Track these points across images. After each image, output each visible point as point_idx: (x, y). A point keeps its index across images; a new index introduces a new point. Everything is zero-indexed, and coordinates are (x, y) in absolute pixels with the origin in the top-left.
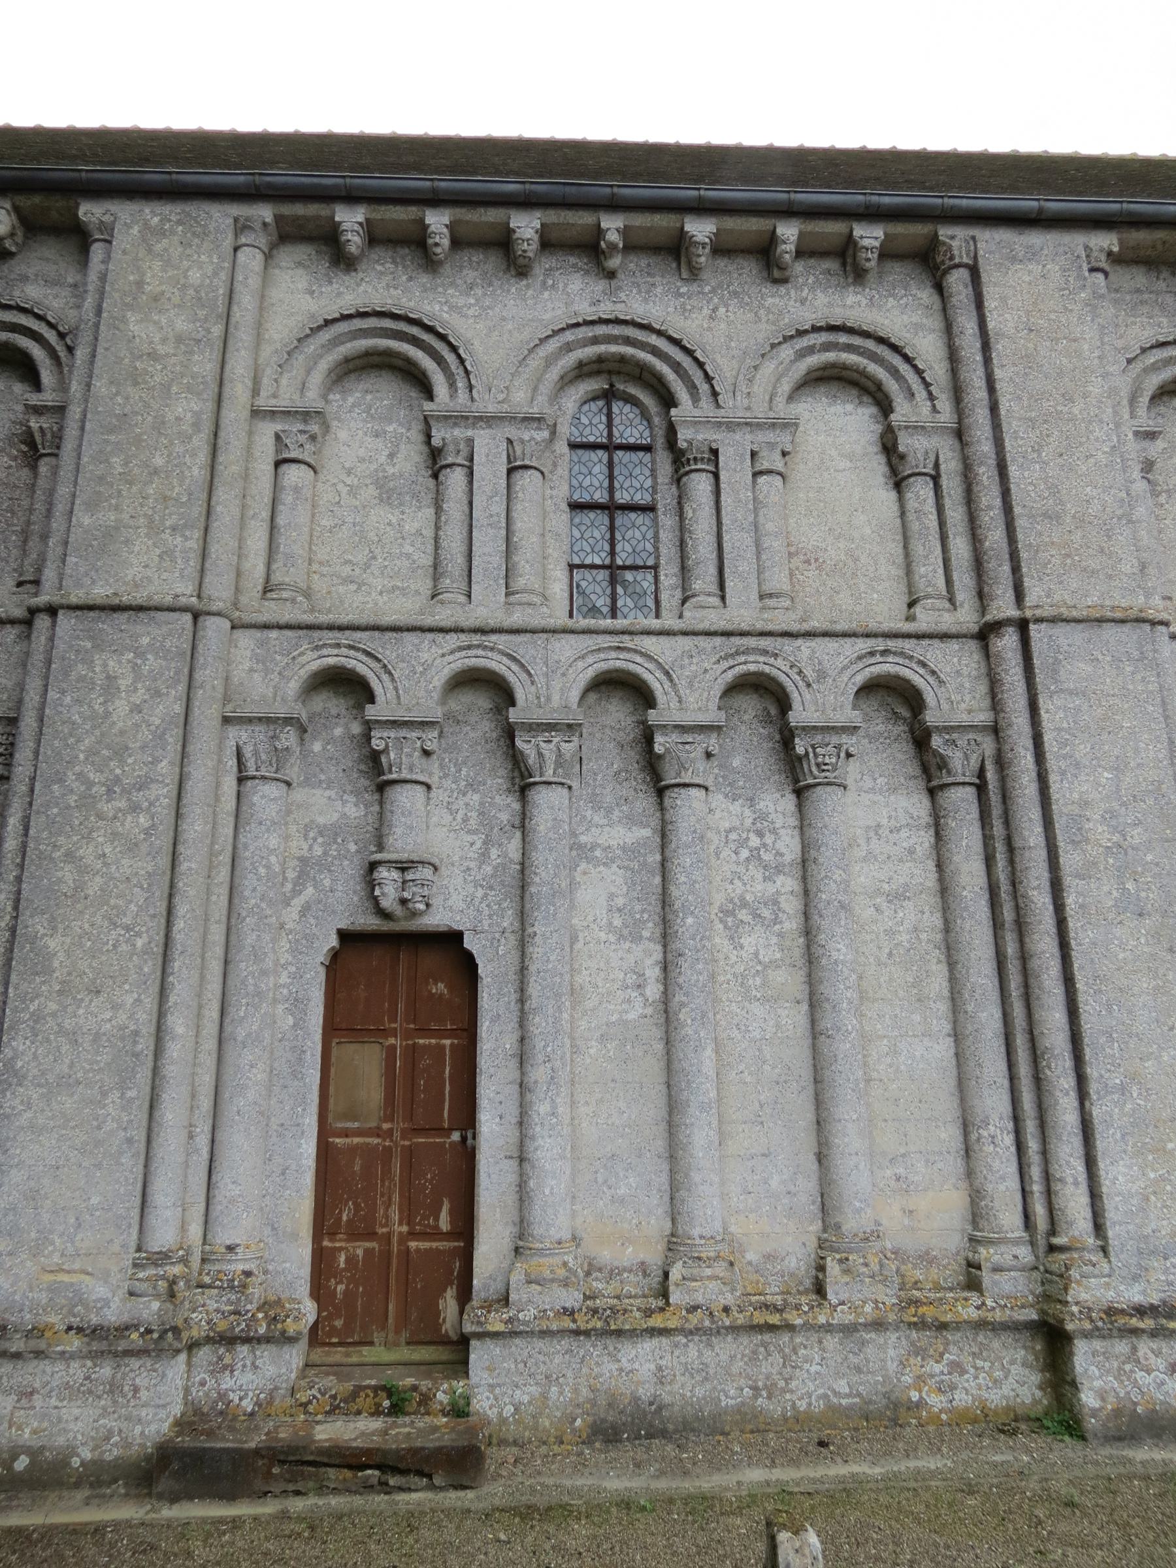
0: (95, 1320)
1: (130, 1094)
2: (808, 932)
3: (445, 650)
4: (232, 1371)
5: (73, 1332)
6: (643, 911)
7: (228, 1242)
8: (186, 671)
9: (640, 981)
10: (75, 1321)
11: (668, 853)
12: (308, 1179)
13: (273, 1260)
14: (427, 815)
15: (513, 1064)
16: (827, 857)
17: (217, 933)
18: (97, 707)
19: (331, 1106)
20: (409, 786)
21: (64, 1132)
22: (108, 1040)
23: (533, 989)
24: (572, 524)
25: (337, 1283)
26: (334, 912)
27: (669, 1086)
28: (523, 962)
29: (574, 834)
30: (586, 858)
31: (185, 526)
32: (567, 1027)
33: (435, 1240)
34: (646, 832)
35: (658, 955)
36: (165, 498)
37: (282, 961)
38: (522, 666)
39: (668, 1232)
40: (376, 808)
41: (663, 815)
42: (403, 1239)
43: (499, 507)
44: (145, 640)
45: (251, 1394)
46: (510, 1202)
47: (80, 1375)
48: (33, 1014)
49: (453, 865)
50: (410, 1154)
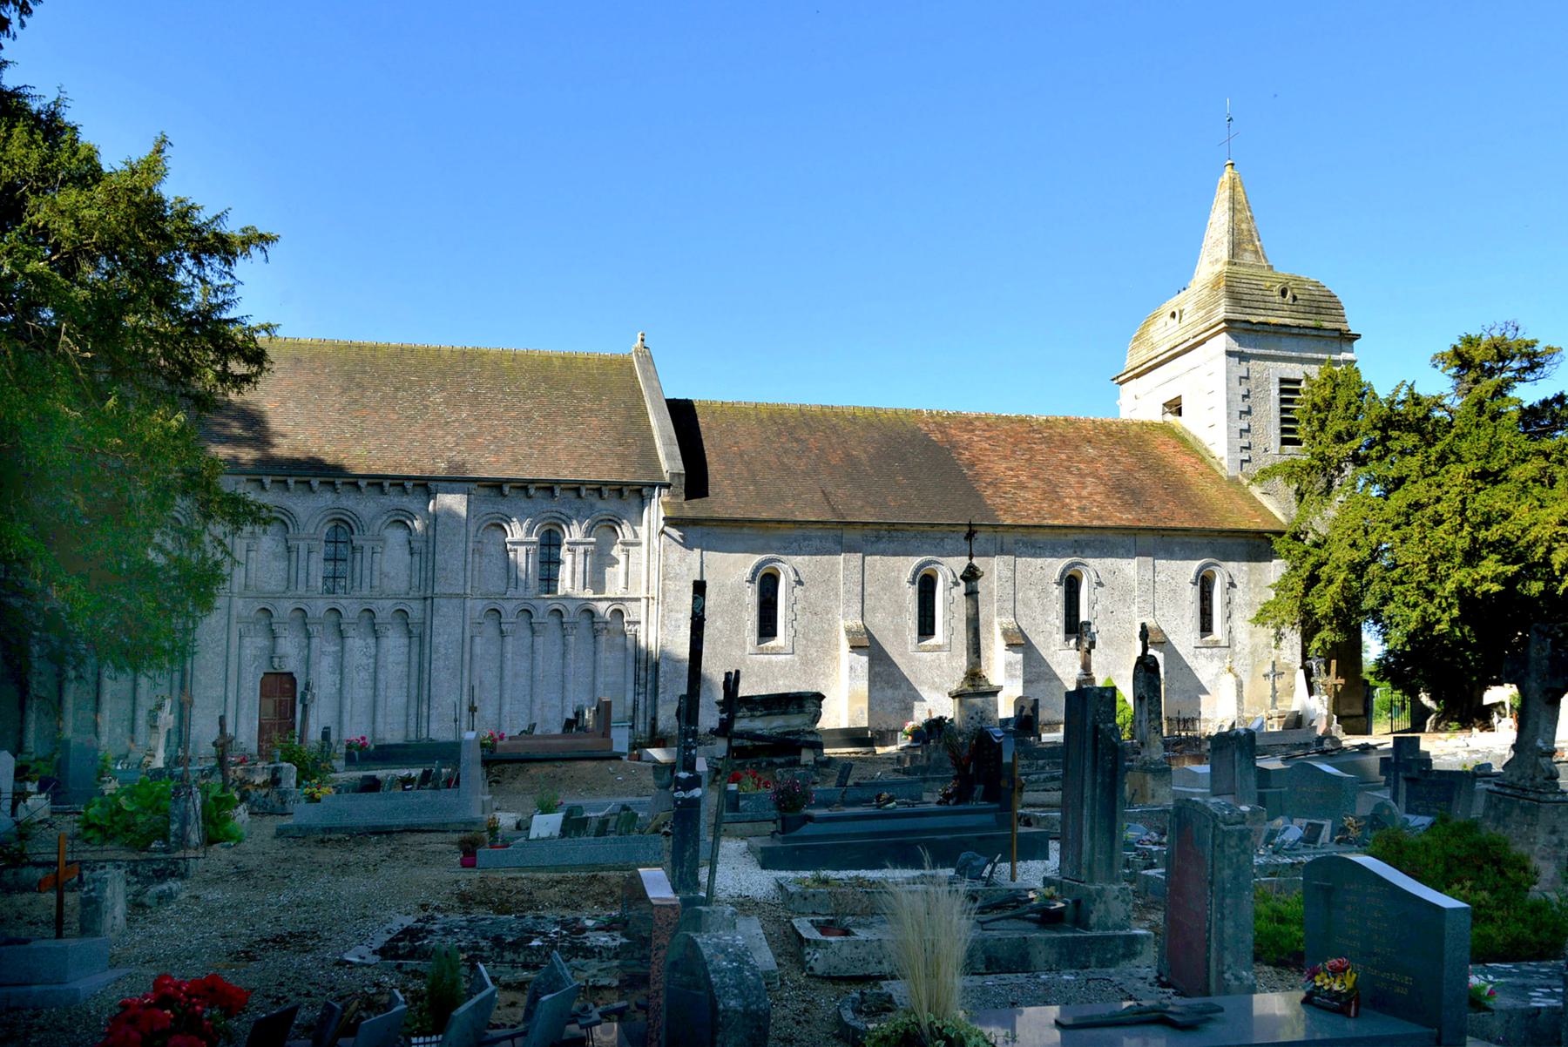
2: (375, 672)
16: (380, 655)
43: (305, 564)
50: (280, 724)
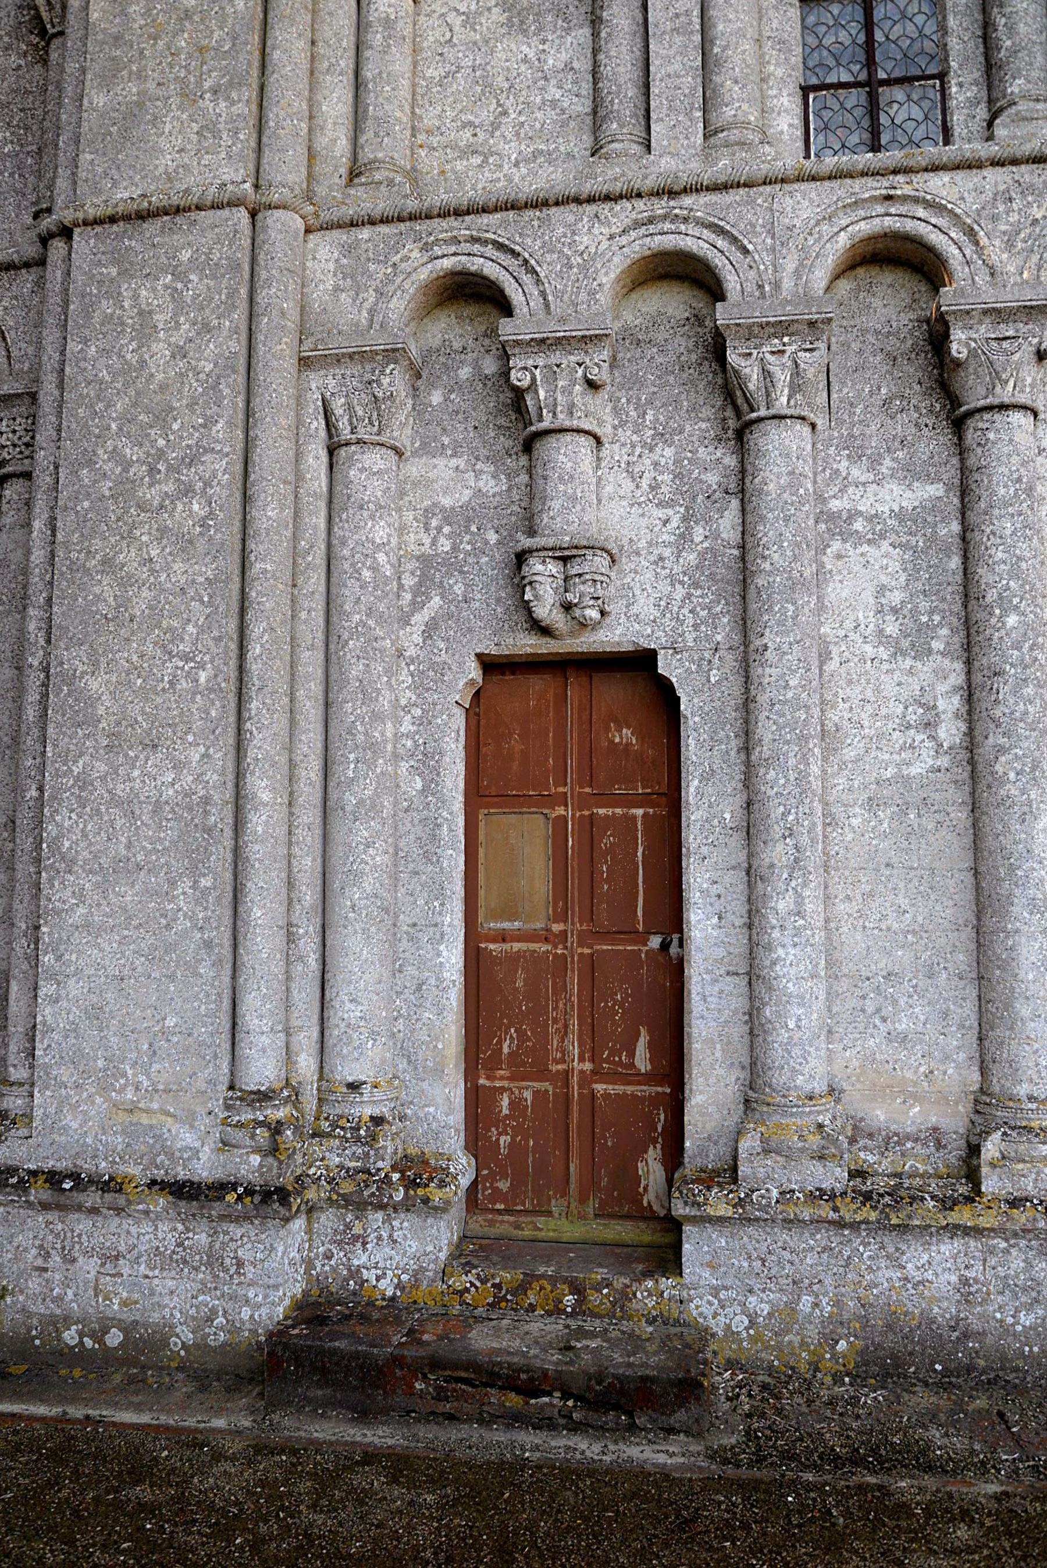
0: (182, 1174)
1: (205, 882)
3: (614, 230)
4: (364, 1244)
5: (157, 1187)
6: (931, 612)
7: (350, 1079)
8: (244, 292)
9: (930, 716)
10: (160, 1174)
11: (972, 517)
12: (454, 997)
13: (411, 1103)
14: (598, 483)
15: (736, 841)
17: (311, 662)
18: (129, 356)
19: (481, 901)
20: (568, 437)
21: (126, 932)
22: (173, 811)
23: (765, 730)
24: (804, 27)
25: (500, 1134)
26: (470, 630)
27: (976, 873)
28: (747, 690)
29: (820, 498)
30: (841, 534)
31: (231, 84)
32: (816, 785)
33: (629, 1083)
34: (935, 490)
35: (957, 677)
36: (201, 50)
37: (403, 702)
38: (734, 240)
39: (976, 1087)
40: (524, 478)
41: (962, 460)
42: (585, 1080)
44: (185, 255)
45: (389, 1273)
46: (736, 1037)
47: (171, 1240)
48: (77, 779)
49: (638, 554)
50: (591, 966)
